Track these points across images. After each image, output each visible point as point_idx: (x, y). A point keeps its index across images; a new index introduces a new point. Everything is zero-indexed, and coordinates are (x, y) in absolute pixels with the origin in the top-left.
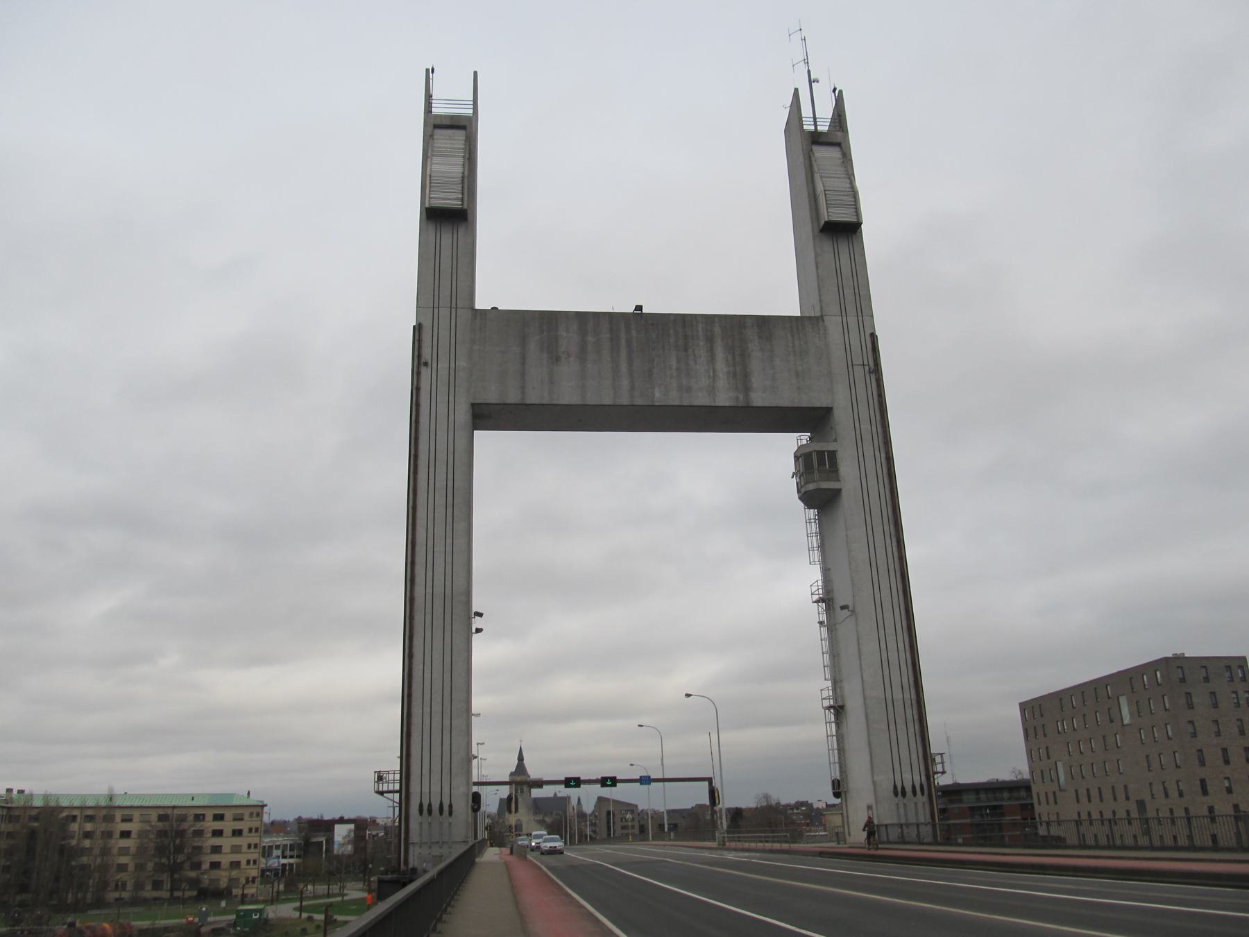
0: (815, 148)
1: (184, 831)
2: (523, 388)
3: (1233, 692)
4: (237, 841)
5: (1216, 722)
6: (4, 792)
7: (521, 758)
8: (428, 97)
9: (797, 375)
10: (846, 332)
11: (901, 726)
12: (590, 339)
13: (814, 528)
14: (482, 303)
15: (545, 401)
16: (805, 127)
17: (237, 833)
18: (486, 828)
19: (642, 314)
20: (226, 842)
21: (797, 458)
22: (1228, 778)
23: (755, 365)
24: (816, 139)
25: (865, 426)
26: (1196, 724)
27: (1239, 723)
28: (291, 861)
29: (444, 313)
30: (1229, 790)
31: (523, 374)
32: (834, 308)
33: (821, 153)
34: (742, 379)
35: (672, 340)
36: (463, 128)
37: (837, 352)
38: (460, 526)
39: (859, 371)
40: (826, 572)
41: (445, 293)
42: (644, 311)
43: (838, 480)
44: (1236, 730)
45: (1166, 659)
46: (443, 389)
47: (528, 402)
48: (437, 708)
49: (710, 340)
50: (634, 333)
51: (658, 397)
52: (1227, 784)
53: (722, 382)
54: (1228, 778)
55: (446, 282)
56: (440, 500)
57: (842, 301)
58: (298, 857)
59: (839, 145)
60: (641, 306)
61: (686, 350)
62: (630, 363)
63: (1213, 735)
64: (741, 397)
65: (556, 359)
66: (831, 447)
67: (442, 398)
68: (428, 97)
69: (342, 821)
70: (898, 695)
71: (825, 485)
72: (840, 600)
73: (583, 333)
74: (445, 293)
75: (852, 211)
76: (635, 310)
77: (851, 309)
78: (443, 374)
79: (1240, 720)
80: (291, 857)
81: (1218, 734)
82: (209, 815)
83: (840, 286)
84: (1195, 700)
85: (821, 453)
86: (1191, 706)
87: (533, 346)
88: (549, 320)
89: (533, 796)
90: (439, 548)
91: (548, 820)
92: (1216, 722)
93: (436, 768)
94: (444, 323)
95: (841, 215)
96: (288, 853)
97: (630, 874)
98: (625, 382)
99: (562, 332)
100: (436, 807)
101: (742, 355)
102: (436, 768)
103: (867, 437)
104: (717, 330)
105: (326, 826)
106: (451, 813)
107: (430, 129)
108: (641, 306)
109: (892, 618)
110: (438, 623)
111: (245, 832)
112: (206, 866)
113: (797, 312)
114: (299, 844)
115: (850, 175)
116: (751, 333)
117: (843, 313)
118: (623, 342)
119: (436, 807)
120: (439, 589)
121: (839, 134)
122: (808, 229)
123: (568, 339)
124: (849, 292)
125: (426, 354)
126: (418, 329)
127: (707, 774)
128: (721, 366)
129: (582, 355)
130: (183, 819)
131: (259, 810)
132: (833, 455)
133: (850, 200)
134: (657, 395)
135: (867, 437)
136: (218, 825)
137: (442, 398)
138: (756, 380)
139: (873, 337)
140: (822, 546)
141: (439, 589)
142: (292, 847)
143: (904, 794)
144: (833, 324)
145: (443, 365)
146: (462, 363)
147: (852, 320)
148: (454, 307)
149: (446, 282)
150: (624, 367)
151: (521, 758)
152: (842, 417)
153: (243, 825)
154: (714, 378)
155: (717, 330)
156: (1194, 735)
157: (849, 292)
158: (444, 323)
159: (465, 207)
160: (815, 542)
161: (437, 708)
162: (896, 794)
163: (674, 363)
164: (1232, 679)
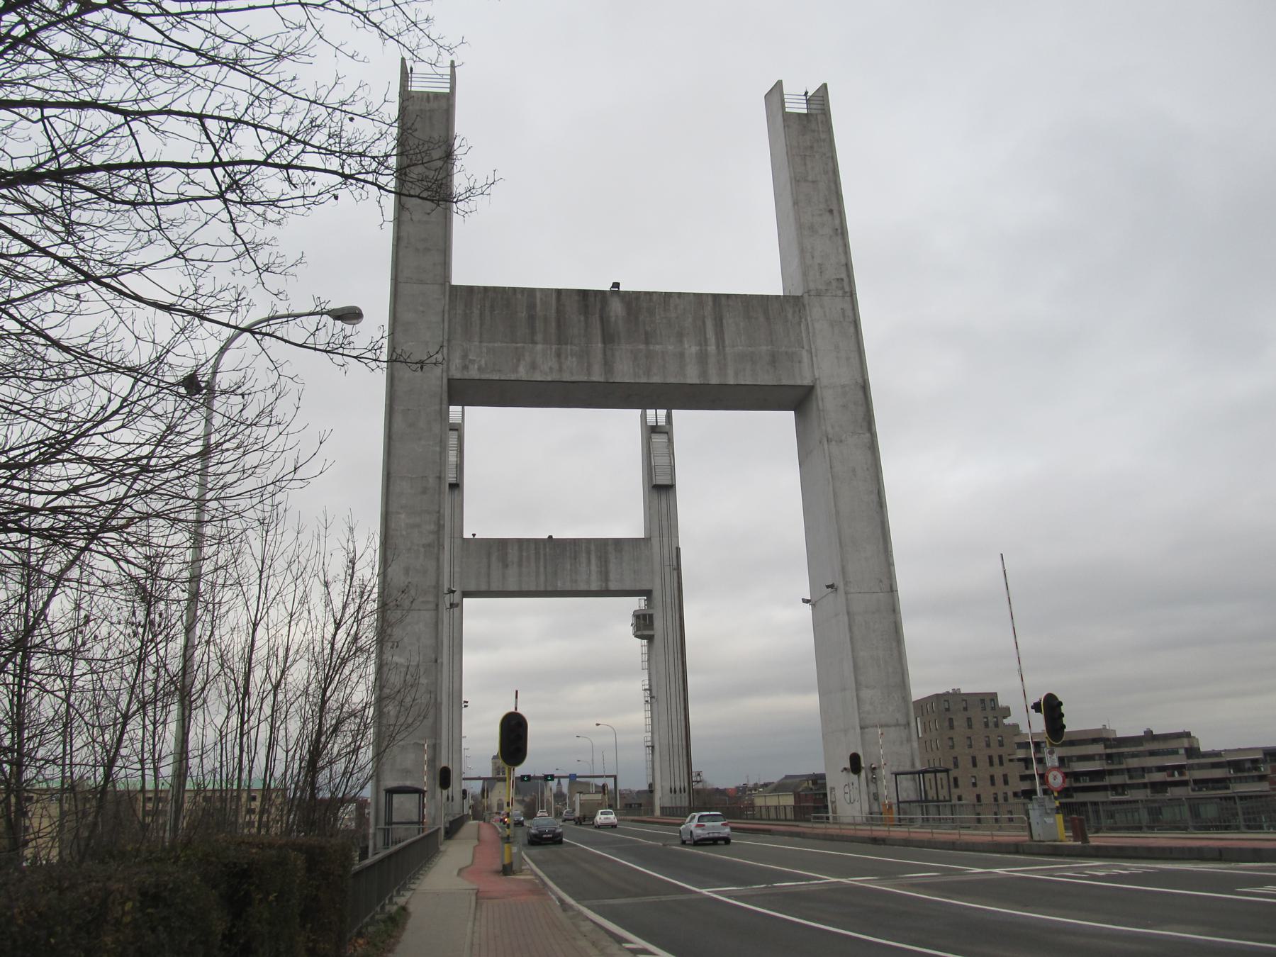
0: (653, 435)
3: (985, 718)
5: (969, 738)
10: (661, 547)
11: (676, 758)
12: (525, 554)
14: (467, 535)
15: (500, 589)
16: (787, 110)
18: (470, 807)
19: (618, 292)
21: (634, 615)
22: (975, 777)
23: (612, 567)
26: (954, 740)
27: (987, 739)
30: (974, 785)
31: (489, 575)
34: (605, 575)
35: (568, 554)
36: (457, 430)
37: (657, 558)
38: (456, 657)
39: (667, 569)
42: (622, 289)
43: (652, 629)
44: (984, 744)
45: (937, 695)
47: (491, 589)
49: (589, 553)
50: (548, 550)
51: (525, 588)
52: (973, 781)
53: (594, 577)
54: (975, 777)
57: (661, 527)
59: (667, 433)
60: (619, 284)
61: (575, 559)
62: (545, 568)
63: (966, 747)
64: (604, 585)
65: (506, 566)
70: (675, 742)
73: (520, 549)
76: (612, 287)
77: (665, 532)
79: (988, 737)
81: (970, 746)
83: (660, 520)
84: (955, 723)
86: (951, 727)
87: (494, 559)
88: (503, 544)
89: (664, 424)
91: (527, 799)
92: (951, 739)
97: (666, 878)
98: (542, 578)
101: (606, 561)
103: (669, 606)
104: (593, 547)
106: (452, 800)
108: (619, 284)
113: (776, 289)
116: (611, 549)
117: (661, 535)
118: (542, 556)
123: (513, 554)
124: (665, 523)
127: (614, 774)
128: (594, 568)
129: (520, 565)
132: (651, 616)
134: (559, 584)
135: (669, 606)
138: (612, 576)
139: (678, 549)
143: (675, 792)
146: (457, 569)
147: (666, 539)
148: (452, 537)
150: (542, 569)
152: (657, 595)
154: (590, 575)
155: (593, 547)
156: (952, 747)
157: (665, 523)
159: (458, 482)
162: (671, 792)
163: (568, 567)
164: (984, 709)
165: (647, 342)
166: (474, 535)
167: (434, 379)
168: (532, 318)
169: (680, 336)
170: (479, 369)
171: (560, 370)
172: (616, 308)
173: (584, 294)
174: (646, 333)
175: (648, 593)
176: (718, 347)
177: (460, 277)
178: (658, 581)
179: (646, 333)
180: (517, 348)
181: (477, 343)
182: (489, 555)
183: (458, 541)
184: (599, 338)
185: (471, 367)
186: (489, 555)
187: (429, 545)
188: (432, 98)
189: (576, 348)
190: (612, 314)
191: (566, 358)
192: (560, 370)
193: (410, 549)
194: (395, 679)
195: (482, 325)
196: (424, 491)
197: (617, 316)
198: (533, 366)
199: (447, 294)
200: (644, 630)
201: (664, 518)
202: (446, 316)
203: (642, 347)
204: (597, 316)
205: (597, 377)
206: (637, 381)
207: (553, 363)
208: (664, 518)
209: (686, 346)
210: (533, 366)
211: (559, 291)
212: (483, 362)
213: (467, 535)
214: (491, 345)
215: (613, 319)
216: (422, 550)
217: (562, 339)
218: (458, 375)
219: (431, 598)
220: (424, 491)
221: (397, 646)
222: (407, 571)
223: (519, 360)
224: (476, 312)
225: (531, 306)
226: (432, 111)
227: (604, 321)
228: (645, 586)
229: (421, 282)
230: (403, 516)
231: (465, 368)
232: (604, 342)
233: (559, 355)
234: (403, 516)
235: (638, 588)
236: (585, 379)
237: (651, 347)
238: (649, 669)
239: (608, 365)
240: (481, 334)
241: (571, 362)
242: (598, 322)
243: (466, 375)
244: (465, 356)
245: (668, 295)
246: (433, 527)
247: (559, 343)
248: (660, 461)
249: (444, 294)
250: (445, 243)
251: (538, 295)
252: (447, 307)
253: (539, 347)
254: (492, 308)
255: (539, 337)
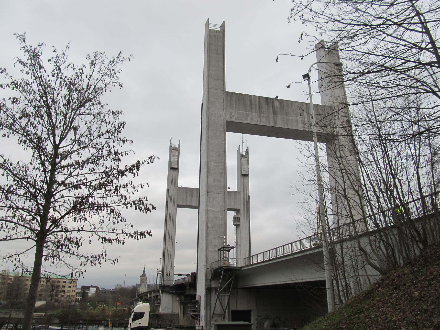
1: (59, 286)
2: (186, 202)
4: (69, 289)
6: (1, 271)
7: (144, 271)
8: (171, 143)
9: (235, 202)
10: (244, 195)
13: (235, 229)
14: (179, 186)
15: (190, 205)
17: (70, 287)
20: (67, 289)
24: (243, 156)
25: (246, 213)
28: (79, 297)
29: (173, 187)
31: (186, 200)
32: (242, 190)
33: (243, 159)
37: (242, 199)
39: (245, 202)
40: (237, 238)
41: (173, 183)
43: (240, 222)
46: (172, 202)
48: (169, 258)
55: (174, 181)
56: (171, 222)
58: (81, 296)
65: (192, 197)
66: (239, 216)
67: (172, 203)
68: (171, 143)
69: (92, 286)
71: (238, 223)
72: (238, 244)
74: (173, 183)
75: (247, 172)
78: (173, 199)
80: (79, 296)
82: (62, 281)
83: (244, 186)
85: (237, 217)
90: (171, 230)
93: (169, 268)
94: (173, 189)
95: (245, 173)
96: (78, 295)
99: (194, 192)
100: (169, 274)
102: (169, 268)
105: (88, 288)
107: (171, 150)
109: (247, 248)
110: (170, 243)
111: (72, 287)
112: (60, 296)
114: (81, 293)
115: (248, 164)
117: (244, 191)
119: (169, 274)
120: (170, 238)
121: (247, 155)
122: (239, 174)
125: (170, 195)
126: (168, 190)
130: (55, 282)
131: (76, 280)
132: (239, 218)
133: (247, 170)
136: (64, 284)
137: (172, 203)
139: (249, 196)
140: (237, 233)
141: (170, 238)
142: (79, 293)
144: (242, 193)
145: (173, 197)
148: (175, 186)
149: (174, 181)
151: (144, 271)
152: (242, 211)
153: (71, 285)
158: (173, 189)
160: (235, 232)
161: (169, 258)
165: (287, 116)
166: (181, 186)
167: (222, 121)
168: (251, 104)
169: (296, 115)
170: (235, 118)
171: (260, 121)
172: (277, 104)
173: (267, 98)
174: (286, 113)
175: (238, 211)
176: (308, 119)
177: (228, 89)
178: (242, 206)
179: (286, 113)
180: (247, 113)
181: (234, 110)
182: (187, 193)
183: (176, 188)
184: (272, 113)
185: (233, 118)
186: (187, 193)
187: (221, 173)
188: (218, 32)
189: (265, 115)
190: (276, 105)
191: (262, 118)
192: (260, 121)
193: (215, 174)
194: (211, 215)
195: (236, 105)
196: (219, 156)
197: (277, 107)
198: (252, 119)
199: (225, 94)
200: (237, 222)
201: (245, 185)
202: (225, 101)
203: (285, 117)
204: (271, 106)
205: (272, 125)
206: (284, 127)
207: (258, 119)
208: (245, 185)
209: (298, 118)
210: (252, 119)
211: (259, 97)
212: (236, 116)
213: (179, 186)
214: (239, 111)
215: (276, 107)
216: (219, 174)
217: (260, 112)
218: (229, 120)
219: (222, 190)
220: (219, 156)
221: (81, 245)
222: (214, 181)
223: (247, 117)
224: (234, 101)
225: (251, 100)
226: (218, 36)
227: (273, 107)
228: (238, 207)
229: (216, 89)
230: (213, 163)
231: (231, 118)
232: (273, 114)
233: (260, 117)
234: (213, 163)
235: (235, 208)
236: (268, 125)
237: (288, 117)
238: (237, 236)
239: (275, 121)
240: (235, 107)
241: (264, 119)
242: (271, 108)
243: (231, 120)
244: (231, 114)
245: (292, 102)
246: (222, 167)
247: (260, 113)
248: (244, 166)
249: (224, 94)
250: (224, 77)
251: (253, 97)
252: (225, 98)
253: (254, 114)
254: (239, 100)
255: (253, 110)
